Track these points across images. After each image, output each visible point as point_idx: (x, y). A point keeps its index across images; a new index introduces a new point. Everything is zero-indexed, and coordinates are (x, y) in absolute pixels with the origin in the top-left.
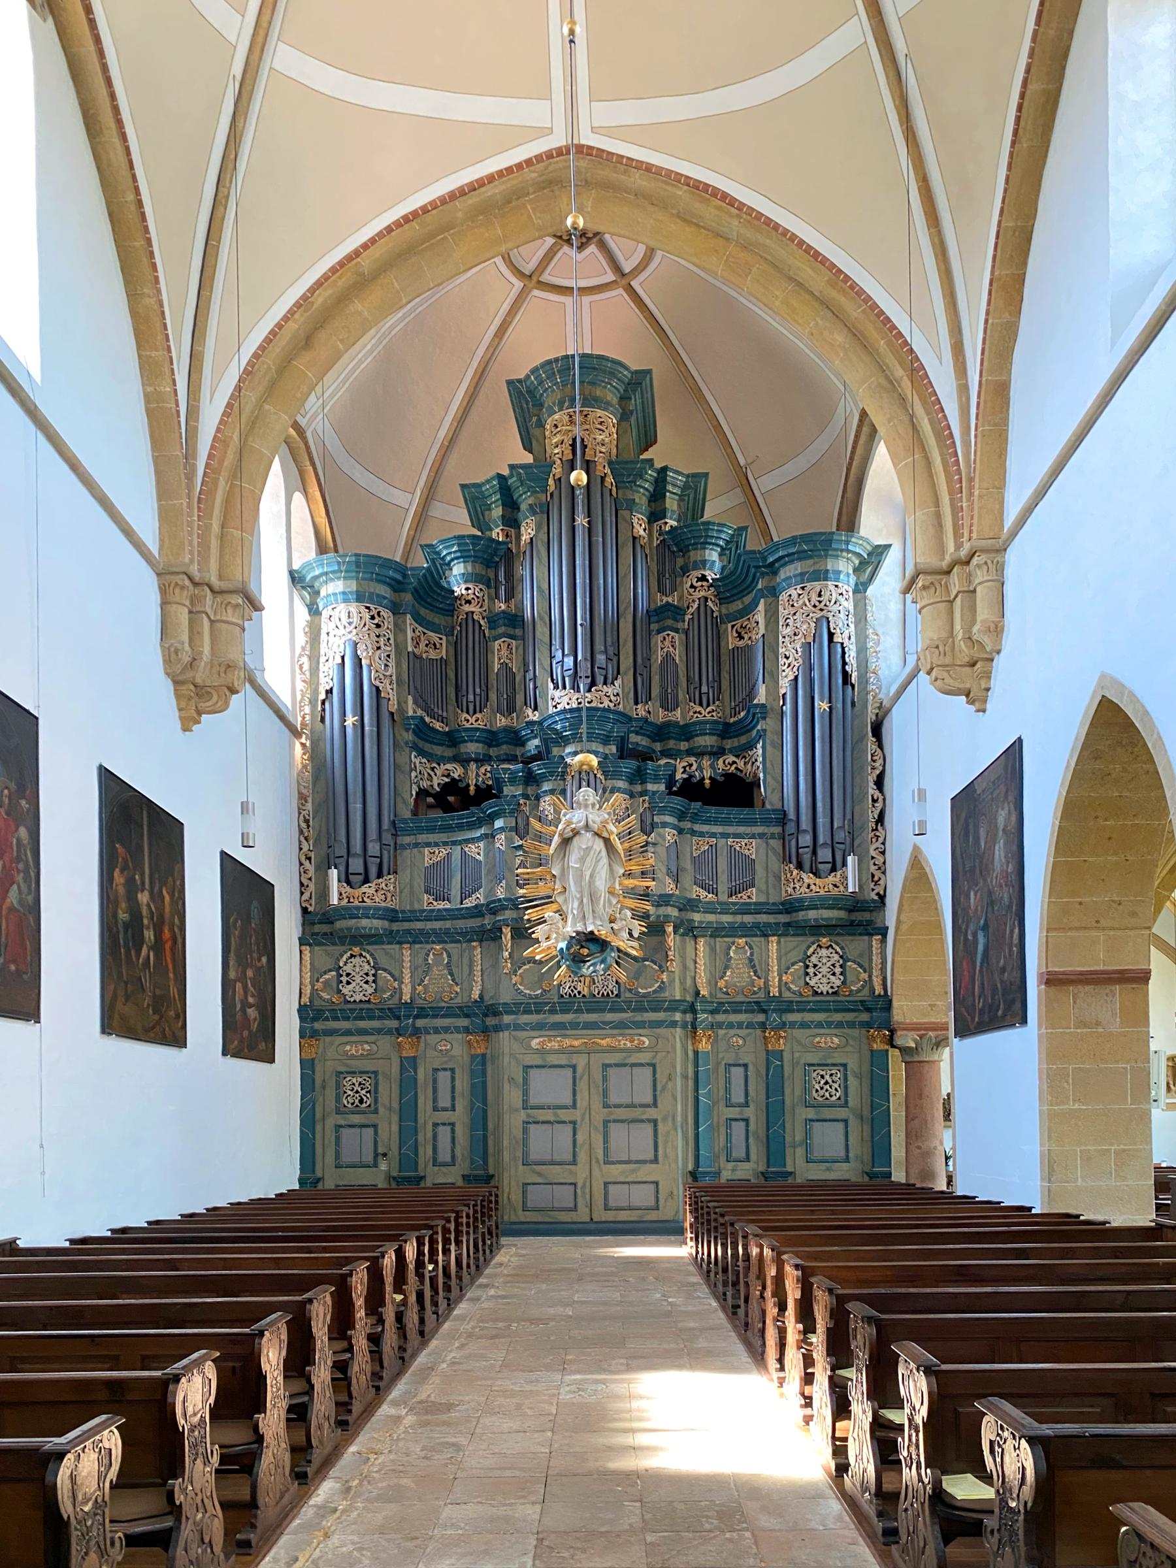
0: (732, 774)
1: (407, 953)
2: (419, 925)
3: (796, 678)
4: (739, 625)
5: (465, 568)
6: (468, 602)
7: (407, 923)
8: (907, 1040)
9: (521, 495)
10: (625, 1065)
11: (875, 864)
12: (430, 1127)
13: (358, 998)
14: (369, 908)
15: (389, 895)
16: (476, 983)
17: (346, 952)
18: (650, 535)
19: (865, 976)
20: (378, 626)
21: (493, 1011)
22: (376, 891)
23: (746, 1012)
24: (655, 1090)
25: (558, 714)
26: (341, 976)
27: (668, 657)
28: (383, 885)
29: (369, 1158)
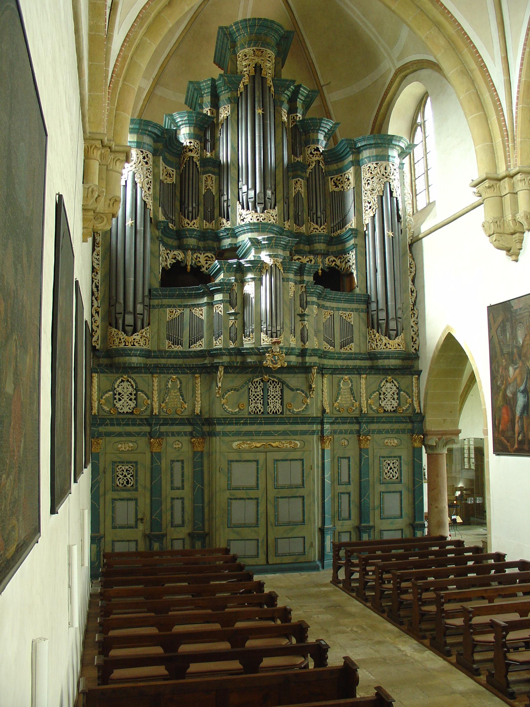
0: (333, 267)
1: (156, 380)
2: (163, 361)
3: (374, 216)
4: (335, 179)
5: (190, 130)
6: (191, 150)
7: (156, 359)
8: (432, 441)
9: (222, 91)
10: (286, 460)
11: (413, 331)
12: (169, 500)
13: (126, 410)
14: (137, 350)
15: (147, 340)
16: (198, 402)
17: (119, 378)
18: (288, 120)
19: (409, 400)
20: (147, 163)
21: (210, 421)
22: (141, 338)
23: (349, 423)
24: (303, 477)
25: (246, 225)
26: (116, 394)
27: (298, 194)
28: (144, 333)
29: (132, 522)
